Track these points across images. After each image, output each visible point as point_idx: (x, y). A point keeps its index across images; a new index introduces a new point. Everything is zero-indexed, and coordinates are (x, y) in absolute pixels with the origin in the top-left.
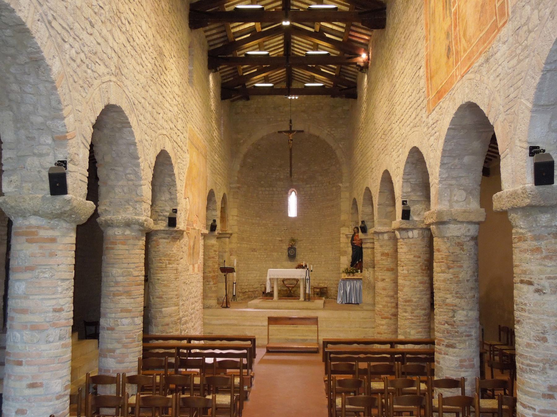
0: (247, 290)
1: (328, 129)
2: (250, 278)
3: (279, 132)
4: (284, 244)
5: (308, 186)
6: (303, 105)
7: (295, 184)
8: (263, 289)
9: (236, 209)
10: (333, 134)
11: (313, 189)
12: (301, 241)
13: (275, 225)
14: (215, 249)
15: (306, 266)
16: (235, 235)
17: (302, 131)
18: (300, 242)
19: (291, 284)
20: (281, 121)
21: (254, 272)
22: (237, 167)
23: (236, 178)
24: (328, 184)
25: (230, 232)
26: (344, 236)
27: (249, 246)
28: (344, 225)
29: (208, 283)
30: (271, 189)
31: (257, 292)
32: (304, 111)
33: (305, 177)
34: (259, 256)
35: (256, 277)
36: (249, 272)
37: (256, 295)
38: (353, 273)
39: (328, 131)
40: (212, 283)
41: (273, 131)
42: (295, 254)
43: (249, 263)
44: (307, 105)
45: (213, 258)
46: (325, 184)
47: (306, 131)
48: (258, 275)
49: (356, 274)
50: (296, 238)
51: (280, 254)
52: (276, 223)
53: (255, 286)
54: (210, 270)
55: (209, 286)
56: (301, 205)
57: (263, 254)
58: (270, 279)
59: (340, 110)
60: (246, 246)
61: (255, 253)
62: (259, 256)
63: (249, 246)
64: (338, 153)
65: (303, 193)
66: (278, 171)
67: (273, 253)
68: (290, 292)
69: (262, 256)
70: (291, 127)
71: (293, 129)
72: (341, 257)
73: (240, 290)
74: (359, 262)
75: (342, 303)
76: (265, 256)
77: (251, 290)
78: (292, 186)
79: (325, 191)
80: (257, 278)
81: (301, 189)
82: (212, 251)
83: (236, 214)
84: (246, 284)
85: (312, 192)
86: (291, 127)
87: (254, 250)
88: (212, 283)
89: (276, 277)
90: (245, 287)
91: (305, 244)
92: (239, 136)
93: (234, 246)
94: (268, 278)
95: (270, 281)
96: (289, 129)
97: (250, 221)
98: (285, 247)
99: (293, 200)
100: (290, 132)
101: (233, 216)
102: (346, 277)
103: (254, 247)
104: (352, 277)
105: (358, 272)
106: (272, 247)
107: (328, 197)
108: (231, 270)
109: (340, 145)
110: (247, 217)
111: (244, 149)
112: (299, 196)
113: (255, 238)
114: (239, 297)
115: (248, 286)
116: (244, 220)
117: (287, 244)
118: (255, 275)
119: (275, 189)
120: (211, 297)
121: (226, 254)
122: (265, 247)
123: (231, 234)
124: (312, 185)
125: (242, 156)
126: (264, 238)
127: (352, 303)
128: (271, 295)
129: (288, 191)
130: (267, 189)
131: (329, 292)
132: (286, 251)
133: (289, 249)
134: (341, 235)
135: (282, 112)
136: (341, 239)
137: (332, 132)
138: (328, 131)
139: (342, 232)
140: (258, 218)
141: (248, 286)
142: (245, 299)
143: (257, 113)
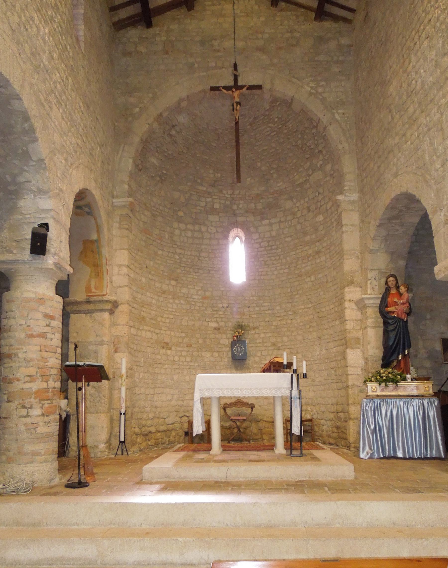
0: (153, 429)
1: (312, 85)
2: (159, 404)
3: (213, 89)
4: (224, 336)
5: (266, 222)
6: (260, 36)
7: (240, 219)
8: (186, 426)
9: (126, 252)
10: (321, 94)
11: (276, 227)
12: (254, 328)
13: (204, 298)
14: (49, 311)
15: (289, 365)
16: (123, 308)
17: (259, 87)
18: (253, 332)
19: (239, 415)
20: (216, 67)
21: (168, 390)
22: (127, 163)
23: (126, 186)
24: (305, 212)
25: (112, 298)
26: (353, 306)
27: (155, 337)
28: (351, 283)
29: (24, 412)
30: (197, 228)
31: (173, 433)
32: (261, 49)
33: (259, 206)
34: (176, 358)
35: (170, 401)
36: (157, 391)
37: (172, 439)
38: (395, 381)
39: (312, 88)
40: (37, 411)
41: (201, 88)
42: (245, 353)
43: (157, 370)
44: (267, 36)
45: (43, 335)
46: (299, 215)
47: (267, 86)
48: (175, 397)
49: (402, 384)
50: (245, 323)
51: (216, 354)
52: (208, 294)
53: (170, 420)
54: (32, 371)
55: (28, 420)
56: (256, 260)
57: (184, 353)
58: (203, 400)
59: (332, 45)
60: (149, 335)
61: (169, 352)
62: (176, 358)
63: (155, 337)
64: (334, 132)
65: (256, 236)
66: (209, 193)
67: (203, 354)
68: (239, 430)
69: (183, 359)
70: (236, 78)
71: (240, 83)
72: (348, 351)
73: (137, 430)
74: (404, 356)
75: (371, 458)
76: (188, 359)
77: (162, 428)
78: (236, 225)
79: (299, 227)
80: (174, 403)
81: (252, 229)
82: (39, 316)
83: (126, 263)
84: (151, 415)
85: (274, 234)
86: (236, 78)
87: (166, 346)
88: (37, 411)
89: (216, 394)
90: (149, 423)
91: (262, 335)
92: (132, 100)
93: (122, 330)
94: (197, 396)
95: (203, 405)
96: (232, 84)
97: (158, 285)
98: (226, 340)
99: (237, 260)
100: (237, 87)
101: (120, 266)
102: (379, 393)
103: (167, 340)
104: (394, 393)
105: (405, 379)
106: (201, 341)
107: (308, 238)
108: (97, 374)
109: (337, 116)
110: (150, 276)
111: (141, 127)
112: (249, 241)
113: (167, 321)
114: (134, 444)
115: (156, 420)
116: (144, 280)
117: (229, 336)
118: (169, 397)
119: (204, 229)
120: (35, 454)
121: (105, 347)
122: (186, 340)
123: (115, 304)
124: (273, 221)
125: (137, 140)
126: (185, 323)
127: (415, 459)
128: (206, 437)
129: (229, 233)
130: (190, 227)
131: (316, 428)
132: (228, 349)
133: (233, 344)
134: (347, 304)
135: (219, 51)
136: (346, 311)
137: (320, 90)
138: (312, 88)
139: (348, 296)
140: (173, 283)
141: (156, 420)
142: (148, 447)
143: (167, 53)
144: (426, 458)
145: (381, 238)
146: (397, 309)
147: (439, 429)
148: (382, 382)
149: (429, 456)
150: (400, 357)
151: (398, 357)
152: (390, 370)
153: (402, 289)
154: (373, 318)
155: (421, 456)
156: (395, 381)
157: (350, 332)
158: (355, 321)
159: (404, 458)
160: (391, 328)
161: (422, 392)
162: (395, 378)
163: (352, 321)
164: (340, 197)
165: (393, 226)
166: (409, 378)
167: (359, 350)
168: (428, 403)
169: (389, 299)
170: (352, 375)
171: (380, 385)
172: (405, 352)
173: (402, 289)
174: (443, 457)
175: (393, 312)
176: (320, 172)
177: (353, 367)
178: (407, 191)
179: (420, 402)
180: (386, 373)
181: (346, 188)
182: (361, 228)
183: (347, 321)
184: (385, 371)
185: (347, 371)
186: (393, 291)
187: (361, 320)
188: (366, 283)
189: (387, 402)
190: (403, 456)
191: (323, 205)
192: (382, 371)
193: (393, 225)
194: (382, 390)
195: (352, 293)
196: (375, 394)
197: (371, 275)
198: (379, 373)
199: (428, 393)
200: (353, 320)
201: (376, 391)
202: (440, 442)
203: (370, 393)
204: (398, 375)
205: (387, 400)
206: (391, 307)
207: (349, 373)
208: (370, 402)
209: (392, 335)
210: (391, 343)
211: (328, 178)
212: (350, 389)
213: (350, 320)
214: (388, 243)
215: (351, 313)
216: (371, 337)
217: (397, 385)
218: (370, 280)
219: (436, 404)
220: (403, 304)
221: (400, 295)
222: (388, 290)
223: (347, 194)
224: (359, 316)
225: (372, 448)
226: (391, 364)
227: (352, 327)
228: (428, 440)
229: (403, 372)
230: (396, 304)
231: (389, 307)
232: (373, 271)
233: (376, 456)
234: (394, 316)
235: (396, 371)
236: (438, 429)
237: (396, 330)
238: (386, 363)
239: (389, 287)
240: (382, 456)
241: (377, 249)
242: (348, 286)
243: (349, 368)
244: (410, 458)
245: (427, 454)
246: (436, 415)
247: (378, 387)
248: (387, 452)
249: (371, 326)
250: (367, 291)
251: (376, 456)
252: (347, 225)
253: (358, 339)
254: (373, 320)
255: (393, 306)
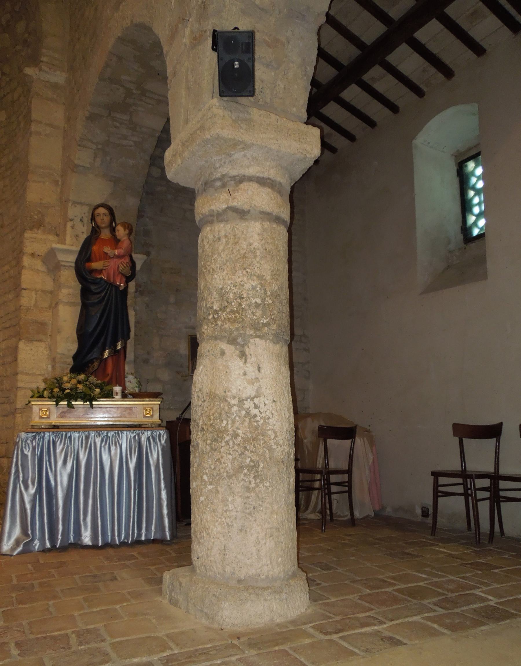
26: (39, 265)
28: (38, 225)
74: (115, 353)
102: (54, 420)
105: (109, 395)
134: (26, 261)
136: (24, 272)
139: (29, 248)
144: (138, 542)
145: (94, 147)
146: (109, 267)
147: (166, 487)
148: (62, 399)
149: (143, 538)
150: (106, 354)
151: (102, 354)
152: (82, 377)
153: (121, 232)
154: (70, 288)
155: (128, 540)
156: (88, 397)
157: (28, 310)
158: (39, 293)
159: (94, 547)
160: (94, 299)
161: (137, 418)
162: (88, 392)
163: (34, 292)
164: (29, 71)
165: (116, 127)
166: (117, 393)
167: (43, 344)
168: (148, 439)
169: (95, 248)
170: (25, 388)
171: (57, 404)
172: (116, 346)
173: (121, 232)
174: (169, 539)
175: (100, 272)
176: (7, 35)
177: (27, 374)
178: (294, 576)
179: (135, 436)
180: (74, 381)
181: (44, 59)
182: (65, 131)
183: (23, 291)
184: (71, 378)
185: (17, 380)
186: (105, 234)
187: (51, 292)
188: (65, 225)
189: (70, 437)
190: (92, 542)
191: (8, 93)
192: (65, 379)
193: (118, 124)
194: (62, 415)
195: (36, 242)
196: (45, 421)
197: (74, 212)
198: (59, 382)
199: (150, 420)
200: (37, 291)
201: (49, 417)
202: (165, 511)
203: (36, 421)
204: (97, 386)
205: (69, 435)
206: (96, 261)
207: (20, 384)
208: (34, 438)
209: (96, 313)
210: (90, 329)
211: (19, 47)
212: (18, 415)
213: (29, 289)
214: (108, 158)
215: (33, 276)
216: (65, 321)
217: (92, 406)
218: (71, 220)
219: (163, 442)
220: (119, 257)
221: (116, 241)
222: (95, 231)
223: (44, 67)
224: (49, 285)
225: (30, 532)
226: (89, 367)
227: (33, 302)
228: (145, 508)
229: (110, 383)
230: (106, 257)
231: (92, 262)
232: (78, 206)
233: (37, 547)
234: (101, 278)
235: (93, 379)
236: (163, 485)
237: (104, 303)
238: (80, 364)
239: (98, 227)
240: (48, 545)
241: (88, 165)
242: (31, 229)
243: (19, 377)
244: (106, 545)
245: (139, 535)
246: (161, 462)
247: (53, 408)
248: (60, 537)
249: (67, 301)
250: (65, 240)
251: (37, 547)
252: (41, 122)
253: (43, 324)
254: (71, 291)
255: (100, 260)
